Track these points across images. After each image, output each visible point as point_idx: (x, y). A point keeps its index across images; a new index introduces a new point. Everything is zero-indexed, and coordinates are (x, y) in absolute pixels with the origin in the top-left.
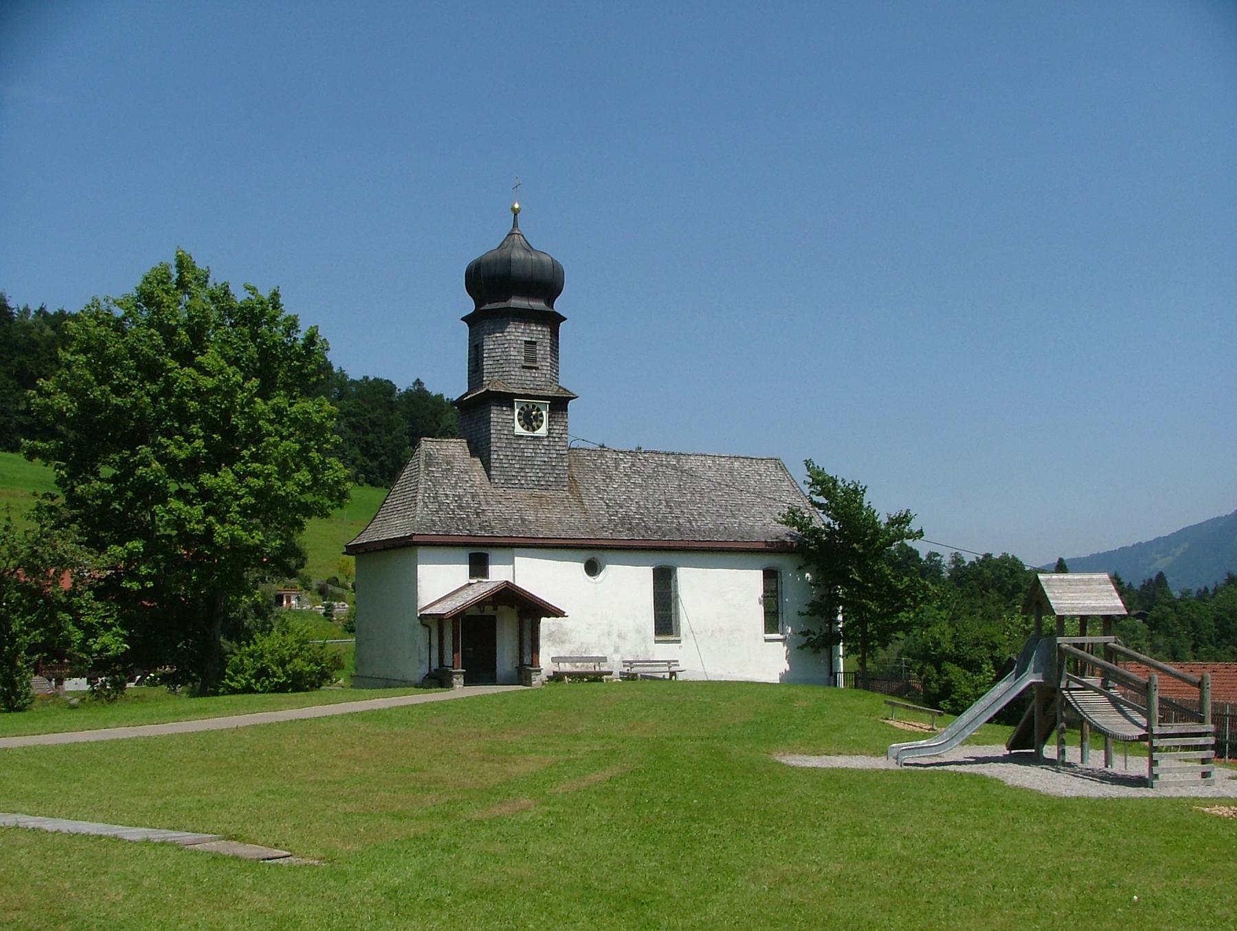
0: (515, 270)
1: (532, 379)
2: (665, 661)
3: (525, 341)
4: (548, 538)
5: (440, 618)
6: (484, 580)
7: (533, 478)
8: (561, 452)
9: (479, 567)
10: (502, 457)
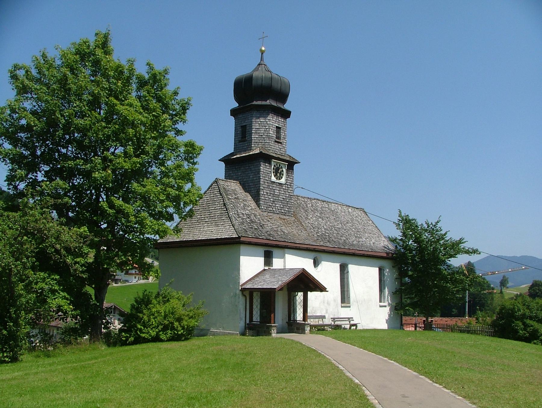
0: (274, 85)
1: (279, 149)
2: (347, 318)
3: (276, 126)
4: (301, 244)
5: (252, 291)
6: (271, 268)
7: (279, 208)
8: (291, 194)
9: (268, 258)
10: (265, 193)
